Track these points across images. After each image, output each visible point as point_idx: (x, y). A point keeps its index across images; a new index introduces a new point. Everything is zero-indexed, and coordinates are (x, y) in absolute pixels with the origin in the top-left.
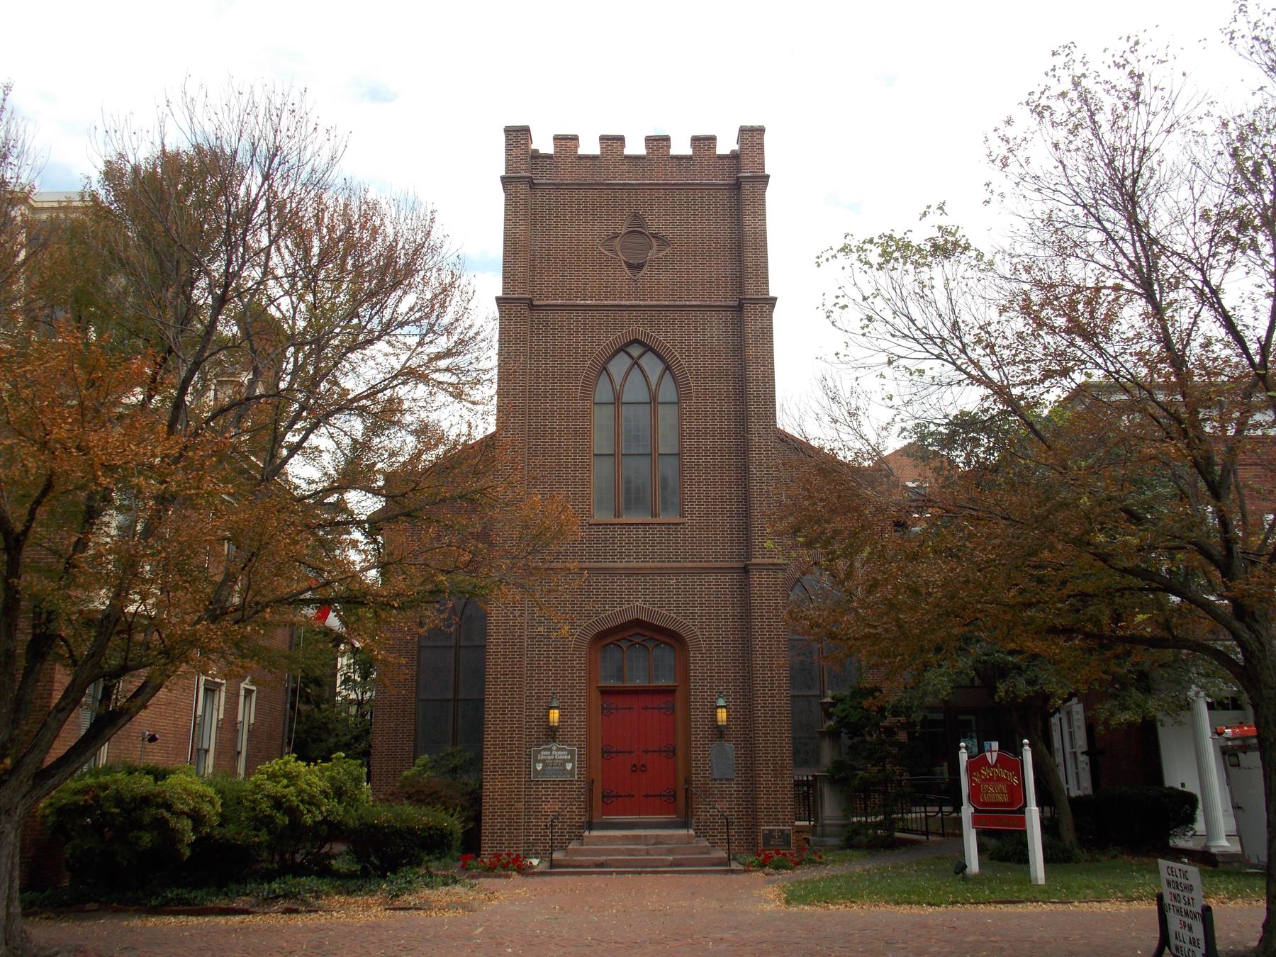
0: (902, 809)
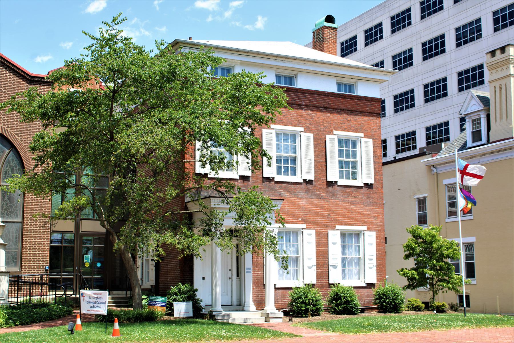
0: (18, 295)
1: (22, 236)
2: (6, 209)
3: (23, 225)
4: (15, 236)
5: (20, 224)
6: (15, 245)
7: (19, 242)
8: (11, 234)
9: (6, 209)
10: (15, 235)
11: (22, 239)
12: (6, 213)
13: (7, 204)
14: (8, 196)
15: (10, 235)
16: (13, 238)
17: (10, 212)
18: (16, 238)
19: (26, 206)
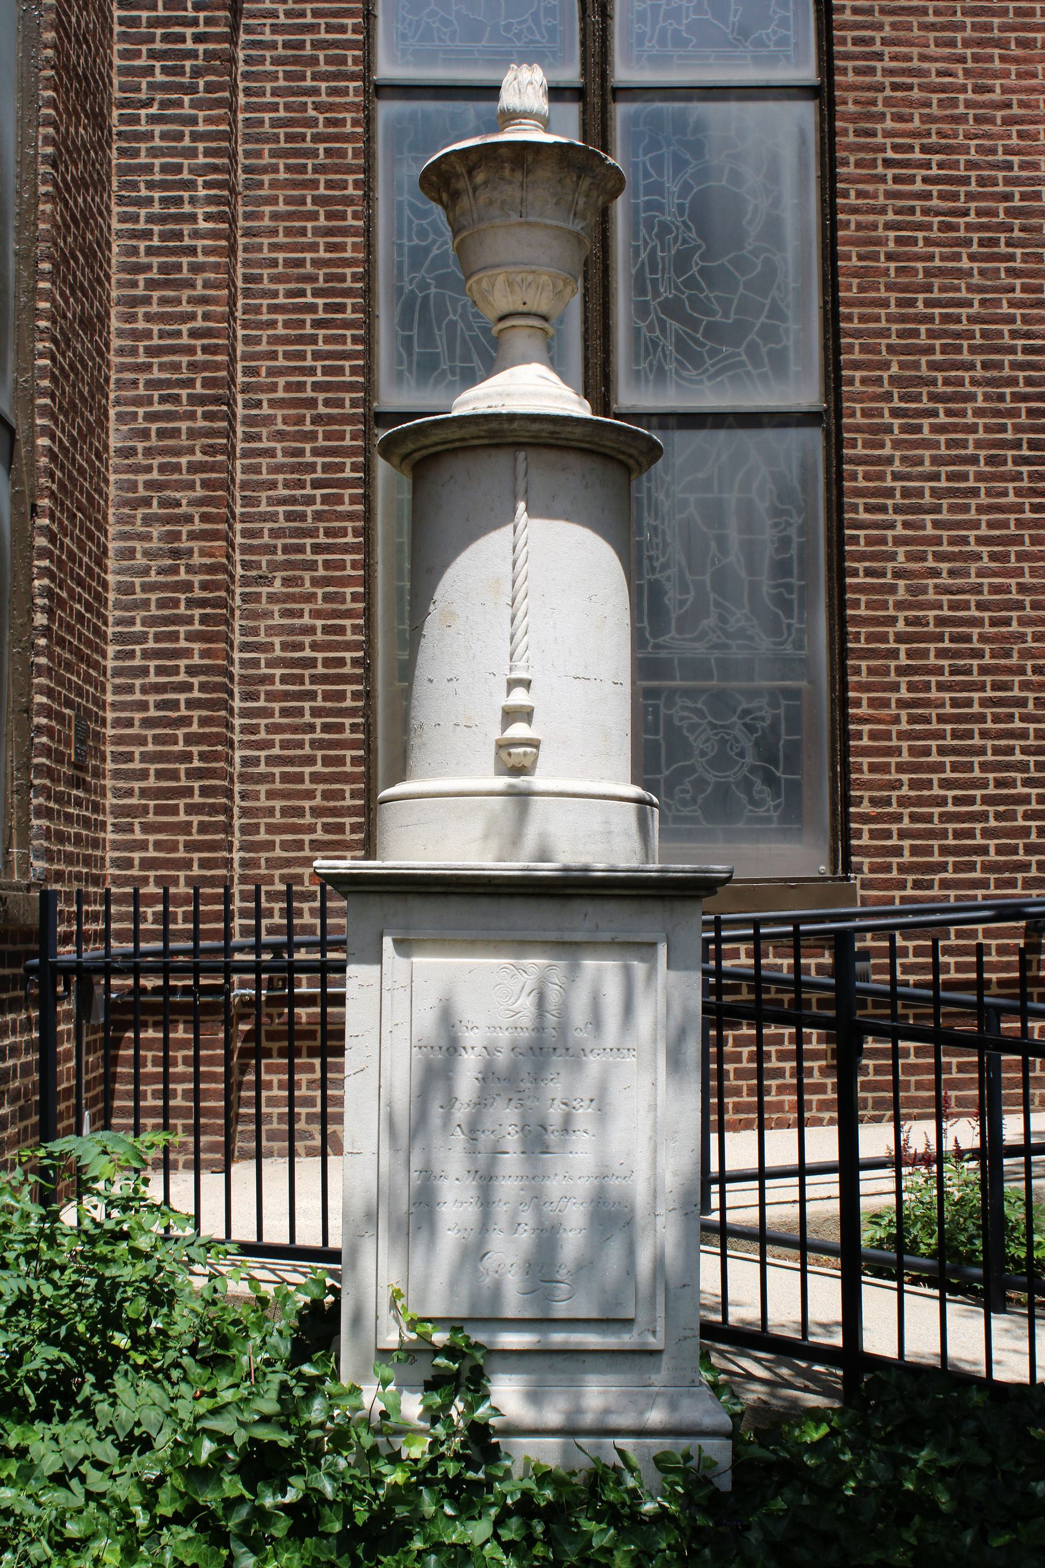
1: (837, 541)
2: (671, 308)
3: (835, 444)
4: (768, 554)
5: (814, 438)
6: (775, 629)
7: (806, 604)
8: (734, 535)
9: (671, 308)
10: (768, 535)
11: (838, 572)
12: (681, 345)
13: (682, 262)
14: (686, 188)
15: (722, 542)
16: (752, 568)
17: (711, 331)
18: (782, 568)
19: (851, 260)
